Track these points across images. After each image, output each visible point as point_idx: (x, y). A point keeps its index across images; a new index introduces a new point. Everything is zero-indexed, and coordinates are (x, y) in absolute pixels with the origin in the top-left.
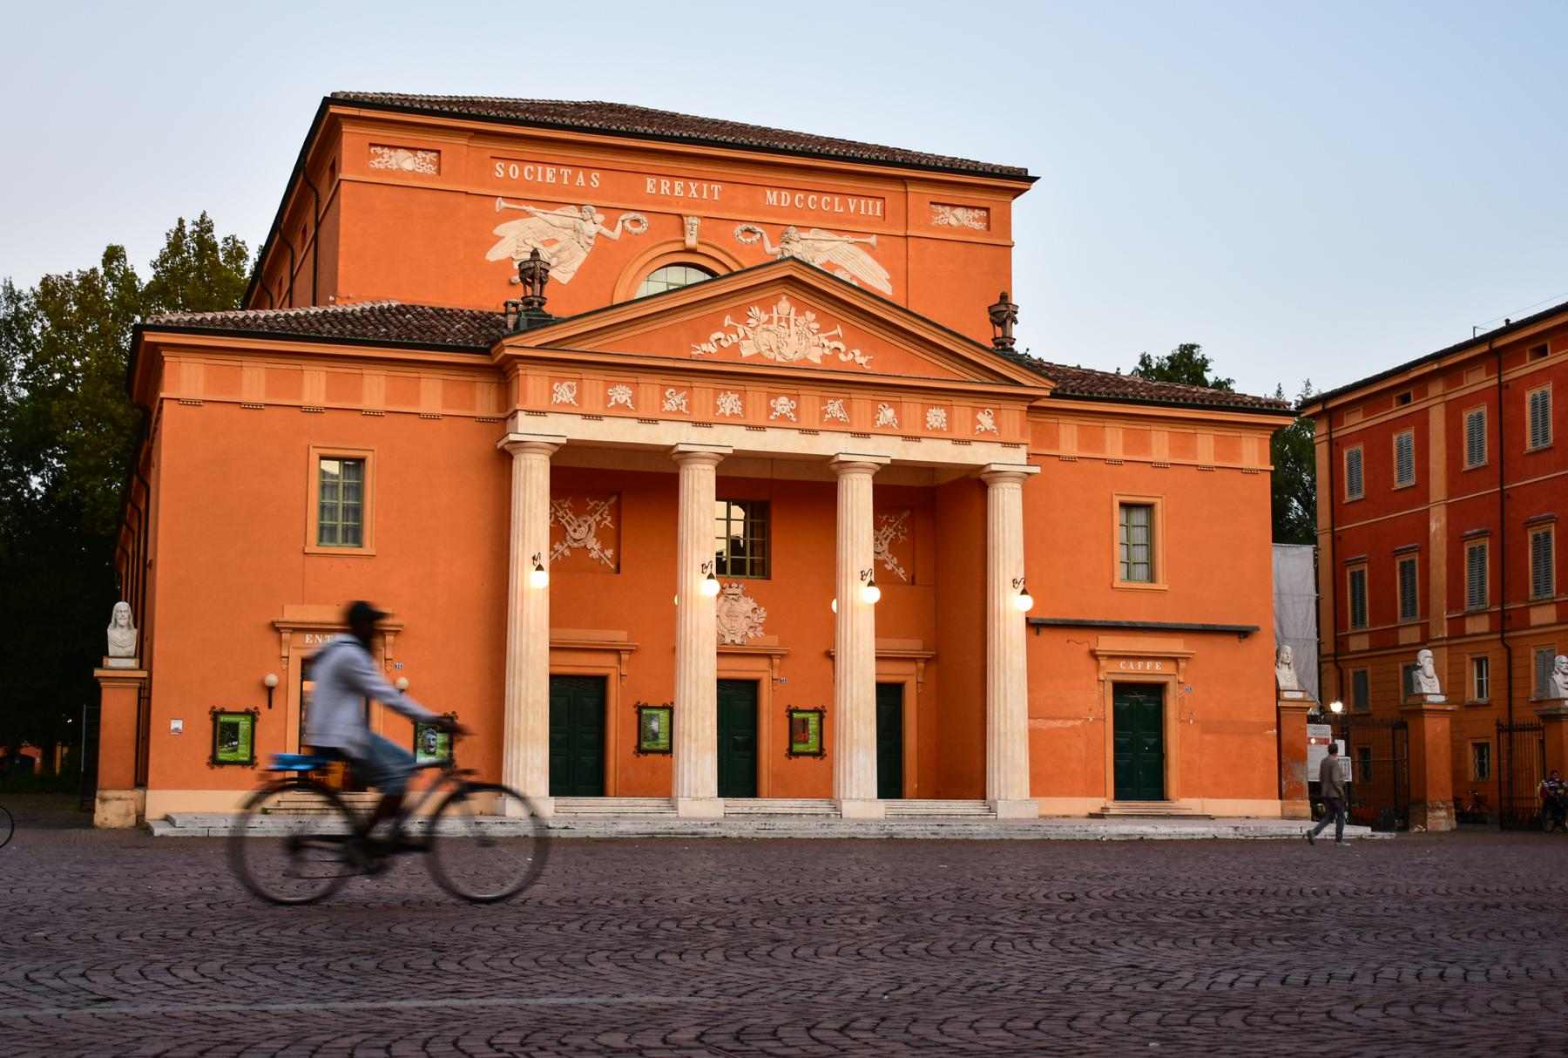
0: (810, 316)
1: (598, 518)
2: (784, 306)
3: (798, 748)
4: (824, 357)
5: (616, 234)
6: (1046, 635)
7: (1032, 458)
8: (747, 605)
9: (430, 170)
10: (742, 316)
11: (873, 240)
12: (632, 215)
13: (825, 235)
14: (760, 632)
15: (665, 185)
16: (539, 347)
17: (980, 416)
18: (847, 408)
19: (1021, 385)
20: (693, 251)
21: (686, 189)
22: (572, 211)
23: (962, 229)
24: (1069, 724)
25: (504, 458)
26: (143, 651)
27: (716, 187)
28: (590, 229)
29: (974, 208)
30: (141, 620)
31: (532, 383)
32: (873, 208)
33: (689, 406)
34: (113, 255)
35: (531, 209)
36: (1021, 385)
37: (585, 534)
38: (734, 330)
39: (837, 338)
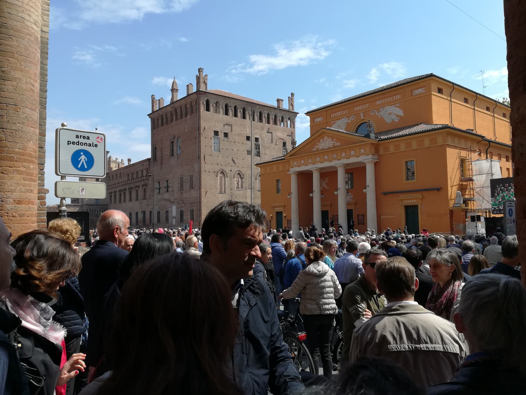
2: (326, 137)
10: (319, 141)
11: (398, 105)
18: (337, 155)
20: (362, 120)
23: (420, 94)
27: (367, 104)
28: (345, 121)
29: (422, 87)
32: (399, 97)
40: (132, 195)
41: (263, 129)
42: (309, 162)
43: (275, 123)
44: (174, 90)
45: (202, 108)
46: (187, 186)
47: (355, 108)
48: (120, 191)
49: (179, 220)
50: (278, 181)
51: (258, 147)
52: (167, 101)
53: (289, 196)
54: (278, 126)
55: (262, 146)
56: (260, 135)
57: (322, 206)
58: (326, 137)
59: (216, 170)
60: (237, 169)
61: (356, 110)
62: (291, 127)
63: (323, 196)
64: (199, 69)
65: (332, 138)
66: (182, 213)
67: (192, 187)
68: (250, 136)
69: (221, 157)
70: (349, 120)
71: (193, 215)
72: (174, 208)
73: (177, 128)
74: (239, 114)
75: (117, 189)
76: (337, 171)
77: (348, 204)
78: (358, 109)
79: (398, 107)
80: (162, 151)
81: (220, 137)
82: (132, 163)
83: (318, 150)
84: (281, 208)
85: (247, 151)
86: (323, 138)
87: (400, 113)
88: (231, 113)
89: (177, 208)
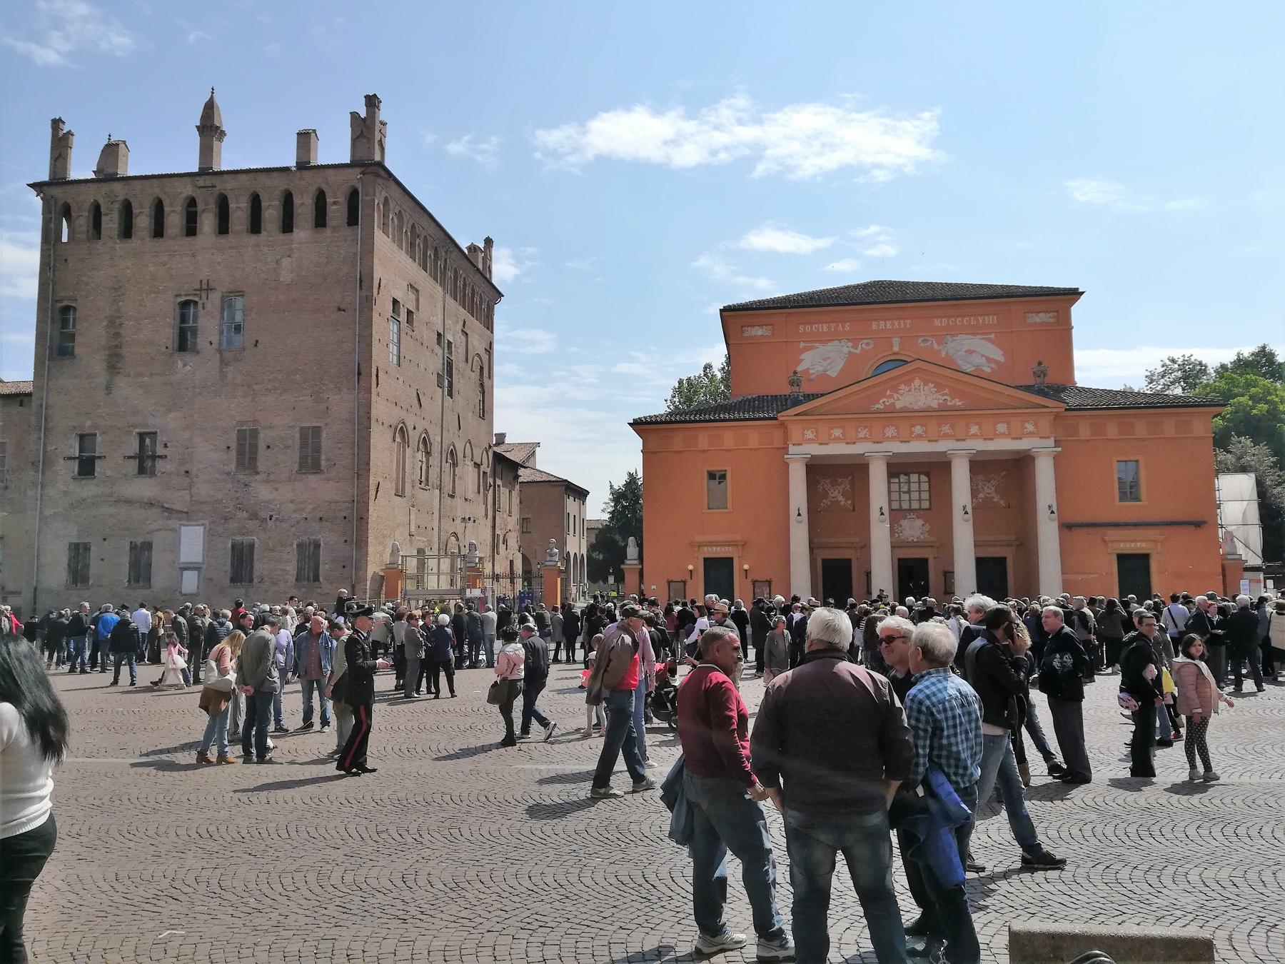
0: (931, 385)
2: (917, 382)
4: (939, 404)
5: (858, 351)
6: (1077, 534)
7: (1057, 443)
8: (919, 522)
9: (769, 333)
10: (895, 389)
11: (992, 336)
13: (965, 337)
15: (882, 324)
17: (1027, 425)
18: (952, 427)
21: (893, 325)
22: (837, 343)
25: (786, 466)
26: (641, 558)
28: (846, 350)
30: (640, 546)
31: (795, 431)
32: (991, 320)
34: (708, 367)
37: (989, 490)
38: (891, 396)
42: (862, 435)
58: (917, 382)
65: (939, 388)
70: (855, 347)
79: (989, 340)
83: (891, 410)
86: (908, 383)
87: (997, 354)
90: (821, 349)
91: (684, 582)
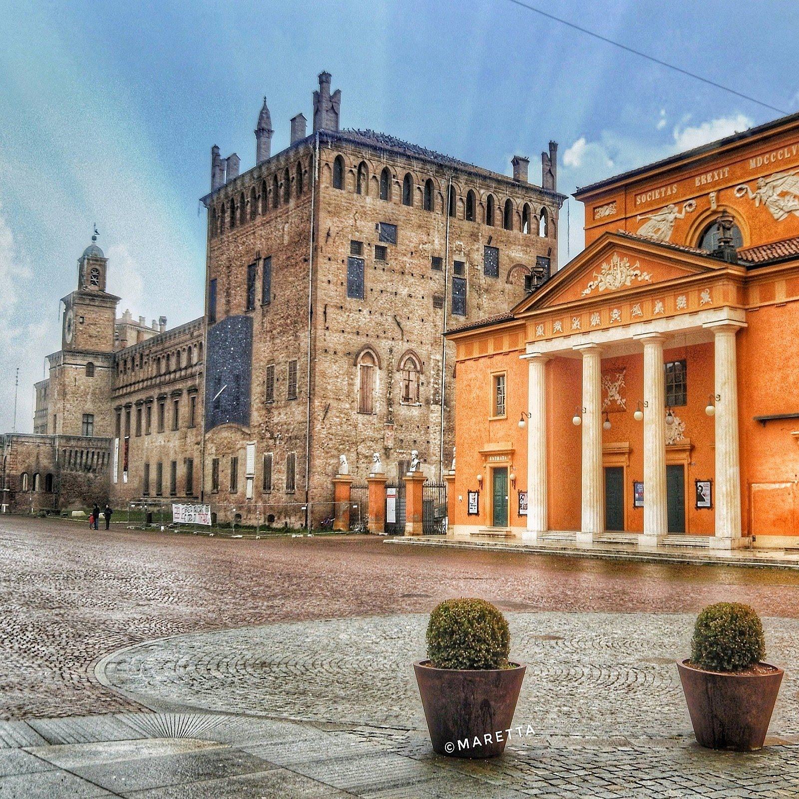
1: (619, 383)
3: (700, 504)
8: (677, 420)
12: (688, 202)
13: (779, 176)
14: (682, 437)
16: (528, 310)
19: (714, 270)
24: (783, 485)
28: (671, 217)
33: (687, 306)
35: (649, 216)
36: (714, 270)
39: (636, 268)
40: (166, 414)
41: (474, 236)
43: (507, 224)
44: (263, 131)
45: (326, 178)
46: (281, 389)
47: (697, 179)
48: (139, 404)
49: (261, 483)
50: (498, 379)
51: (459, 287)
52: (247, 162)
53: (521, 424)
54: (515, 231)
55: (472, 286)
56: (467, 255)
57: (606, 454)
59: (354, 349)
60: (406, 346)
61: (697, 184)
62: (546, 234)
63: (607, 425)
64: (320, 76)
66: (267, 465)
67: (293, 395)
68: (442, 255)
69: (365, 312)
70: (680, 212)
71: (293, 472)
72: (251, 450)
73: (272, 231)
74: (417, 196)
75: (134, 399)
76: (640, 357)
77: (670, 449)
78: (704, 181)
80: (228, 295)
81: (365, 257)
82: (168, 327)
84: (503, 458)
85: (435, 298)
88: (396, 191)
89: (258, 451)
90: (655, 218)
91: (478, 492)
